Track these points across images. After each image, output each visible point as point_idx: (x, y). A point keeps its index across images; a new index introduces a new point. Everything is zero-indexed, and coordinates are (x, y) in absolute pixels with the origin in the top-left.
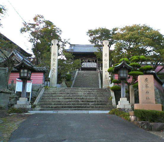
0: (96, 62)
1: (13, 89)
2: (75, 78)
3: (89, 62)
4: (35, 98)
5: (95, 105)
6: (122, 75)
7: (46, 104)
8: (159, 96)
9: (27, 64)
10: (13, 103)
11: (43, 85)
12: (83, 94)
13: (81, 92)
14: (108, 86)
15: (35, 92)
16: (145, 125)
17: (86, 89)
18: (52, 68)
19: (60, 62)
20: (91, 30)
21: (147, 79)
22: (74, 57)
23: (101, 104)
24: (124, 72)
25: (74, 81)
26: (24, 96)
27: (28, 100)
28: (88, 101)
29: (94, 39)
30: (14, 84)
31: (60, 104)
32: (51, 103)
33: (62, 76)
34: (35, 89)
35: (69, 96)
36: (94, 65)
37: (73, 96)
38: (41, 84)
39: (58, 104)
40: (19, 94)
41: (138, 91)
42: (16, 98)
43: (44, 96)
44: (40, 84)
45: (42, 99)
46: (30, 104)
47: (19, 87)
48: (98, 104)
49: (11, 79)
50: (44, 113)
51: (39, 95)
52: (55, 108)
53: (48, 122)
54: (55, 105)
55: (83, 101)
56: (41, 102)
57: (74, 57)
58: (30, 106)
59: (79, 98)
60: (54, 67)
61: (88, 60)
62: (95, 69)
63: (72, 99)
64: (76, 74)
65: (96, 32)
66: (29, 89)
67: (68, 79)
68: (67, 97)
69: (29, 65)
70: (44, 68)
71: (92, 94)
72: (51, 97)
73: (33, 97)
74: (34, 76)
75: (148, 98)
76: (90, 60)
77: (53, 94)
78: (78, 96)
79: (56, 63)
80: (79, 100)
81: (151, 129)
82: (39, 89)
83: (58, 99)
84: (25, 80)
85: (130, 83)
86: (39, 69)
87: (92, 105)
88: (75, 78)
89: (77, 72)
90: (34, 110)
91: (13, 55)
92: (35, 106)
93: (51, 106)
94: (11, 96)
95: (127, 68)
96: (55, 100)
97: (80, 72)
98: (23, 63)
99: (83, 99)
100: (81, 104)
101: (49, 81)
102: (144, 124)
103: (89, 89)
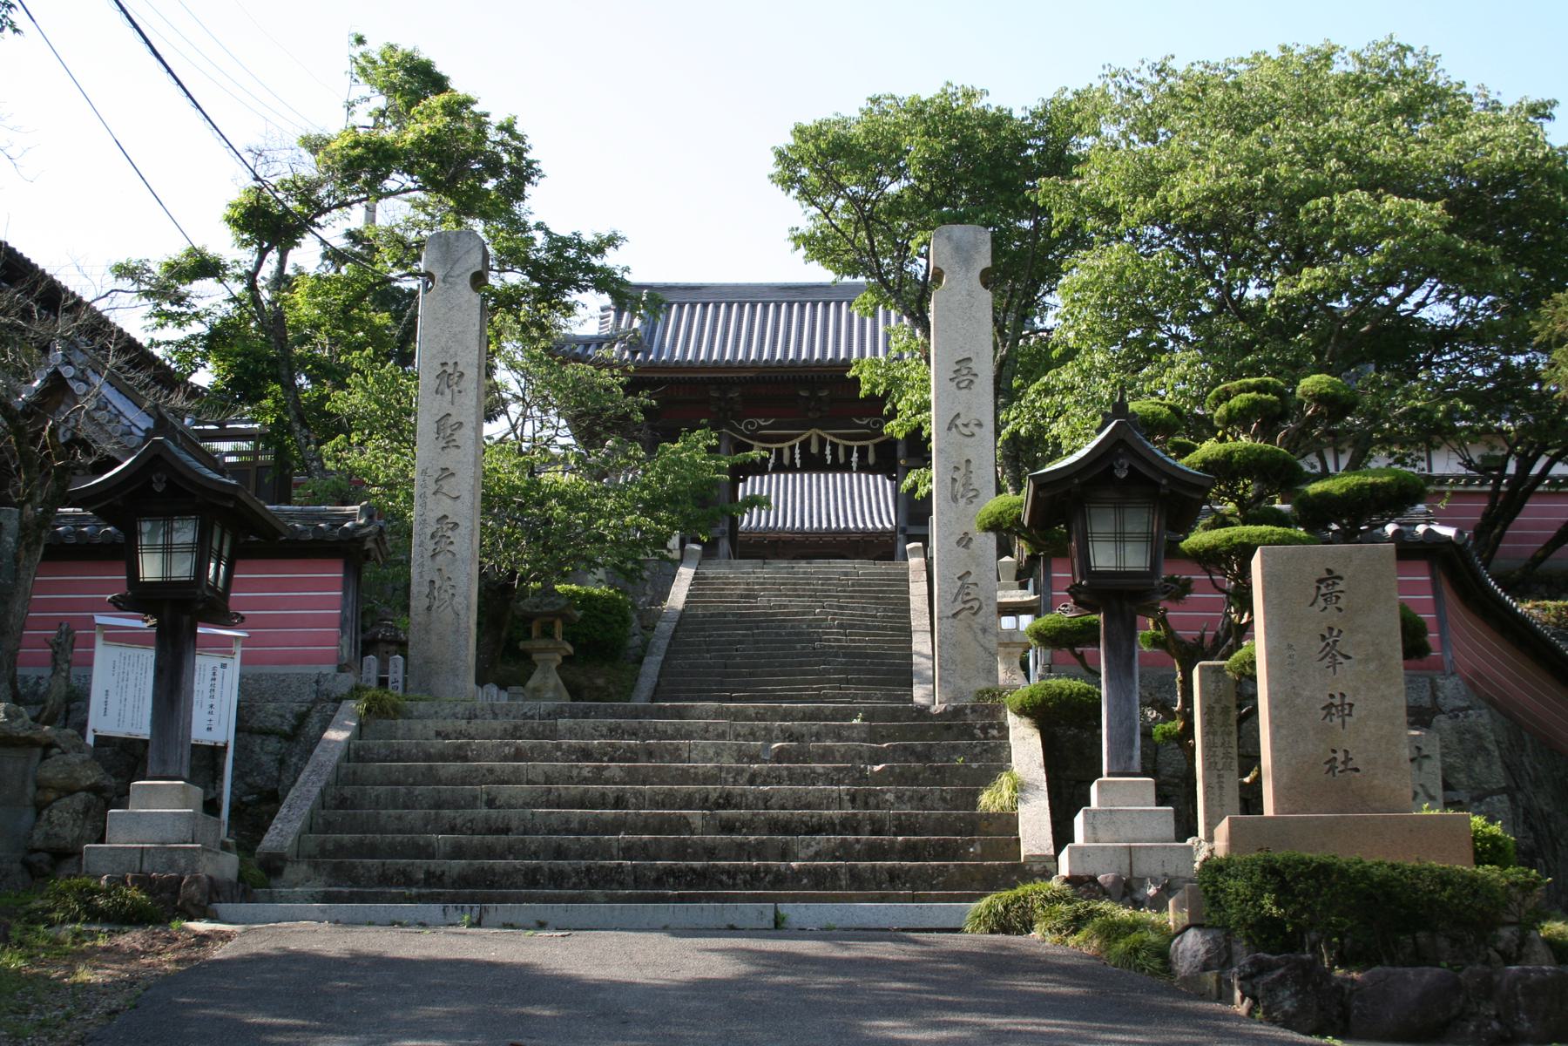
1: (75, 703)
3: (814, 464)
4: (272, 798)
5: (846, 852)
6: (1103, 558)
7: (373, 851)
8: (1498, 768)
9: (195, 464)
10: (69, 833)
11: (347, 680)
12: (728, 762)
13: (713, 743)
15: (273, 744)
16: (1281, 981)
17: (760, 717)
21: (1331, 577)
22: (646, 410)
23: (911, 851)
24: (1128, 528)
25: (651, 667)
26: (171, 772)
27: (211, 807)
28: (775, 826)
30: (74, 670)
31: (509, 851)
32: (421, 839)
34: (273, 713)
35: (598, 777)
36: (862, 501)
37: (632, 777)
38: (329, 669)
39: (490, 853)
40: (126, 760)
41: (1250, 690)
42: (95, 789)
43: (354, 779)
44: (313, 670)
45: (341, 798)
46: (225, 847)
47: (120, 692)
48: (875, 852)
49: (45, 623)
51: (308, 769)
52: (464, 880)
53: (526, 306)
54: (457, 852)
55: (728, 827)
56: (329, 827)
57: (646, 410)
58: (227, 865)
59: (690, 796)
60: (446, 506)
61: (805, 446)
62: (879, 546)
63: (619, 802)
66: (213, 713)
68: (576, 789)
69: (216, 476)
71: (825, 756)
72: (419, 789)
73: (252, 788)
74: (260, 588)
75: (1340, 756)
77: (443, 757)
78: (685, 777)
80: (695, 815)
81: (1347, 1020)
82: (302, 718)
83: (491, 803)
84: (178, 618)
85: (1208, 642)
86: (303, 516)
87: (817, 856)
90: (272, 901)
91: (57, 387)
92: (273, 867)
93: (419, 866)
94: (52, 771)
95: (1158, 485)
96: (460, 816)
98: (158, 457)
99: (727, 801)
100: (711, 852)
101: (402, 647)
102: (1281, 971)
103: (786, 716)
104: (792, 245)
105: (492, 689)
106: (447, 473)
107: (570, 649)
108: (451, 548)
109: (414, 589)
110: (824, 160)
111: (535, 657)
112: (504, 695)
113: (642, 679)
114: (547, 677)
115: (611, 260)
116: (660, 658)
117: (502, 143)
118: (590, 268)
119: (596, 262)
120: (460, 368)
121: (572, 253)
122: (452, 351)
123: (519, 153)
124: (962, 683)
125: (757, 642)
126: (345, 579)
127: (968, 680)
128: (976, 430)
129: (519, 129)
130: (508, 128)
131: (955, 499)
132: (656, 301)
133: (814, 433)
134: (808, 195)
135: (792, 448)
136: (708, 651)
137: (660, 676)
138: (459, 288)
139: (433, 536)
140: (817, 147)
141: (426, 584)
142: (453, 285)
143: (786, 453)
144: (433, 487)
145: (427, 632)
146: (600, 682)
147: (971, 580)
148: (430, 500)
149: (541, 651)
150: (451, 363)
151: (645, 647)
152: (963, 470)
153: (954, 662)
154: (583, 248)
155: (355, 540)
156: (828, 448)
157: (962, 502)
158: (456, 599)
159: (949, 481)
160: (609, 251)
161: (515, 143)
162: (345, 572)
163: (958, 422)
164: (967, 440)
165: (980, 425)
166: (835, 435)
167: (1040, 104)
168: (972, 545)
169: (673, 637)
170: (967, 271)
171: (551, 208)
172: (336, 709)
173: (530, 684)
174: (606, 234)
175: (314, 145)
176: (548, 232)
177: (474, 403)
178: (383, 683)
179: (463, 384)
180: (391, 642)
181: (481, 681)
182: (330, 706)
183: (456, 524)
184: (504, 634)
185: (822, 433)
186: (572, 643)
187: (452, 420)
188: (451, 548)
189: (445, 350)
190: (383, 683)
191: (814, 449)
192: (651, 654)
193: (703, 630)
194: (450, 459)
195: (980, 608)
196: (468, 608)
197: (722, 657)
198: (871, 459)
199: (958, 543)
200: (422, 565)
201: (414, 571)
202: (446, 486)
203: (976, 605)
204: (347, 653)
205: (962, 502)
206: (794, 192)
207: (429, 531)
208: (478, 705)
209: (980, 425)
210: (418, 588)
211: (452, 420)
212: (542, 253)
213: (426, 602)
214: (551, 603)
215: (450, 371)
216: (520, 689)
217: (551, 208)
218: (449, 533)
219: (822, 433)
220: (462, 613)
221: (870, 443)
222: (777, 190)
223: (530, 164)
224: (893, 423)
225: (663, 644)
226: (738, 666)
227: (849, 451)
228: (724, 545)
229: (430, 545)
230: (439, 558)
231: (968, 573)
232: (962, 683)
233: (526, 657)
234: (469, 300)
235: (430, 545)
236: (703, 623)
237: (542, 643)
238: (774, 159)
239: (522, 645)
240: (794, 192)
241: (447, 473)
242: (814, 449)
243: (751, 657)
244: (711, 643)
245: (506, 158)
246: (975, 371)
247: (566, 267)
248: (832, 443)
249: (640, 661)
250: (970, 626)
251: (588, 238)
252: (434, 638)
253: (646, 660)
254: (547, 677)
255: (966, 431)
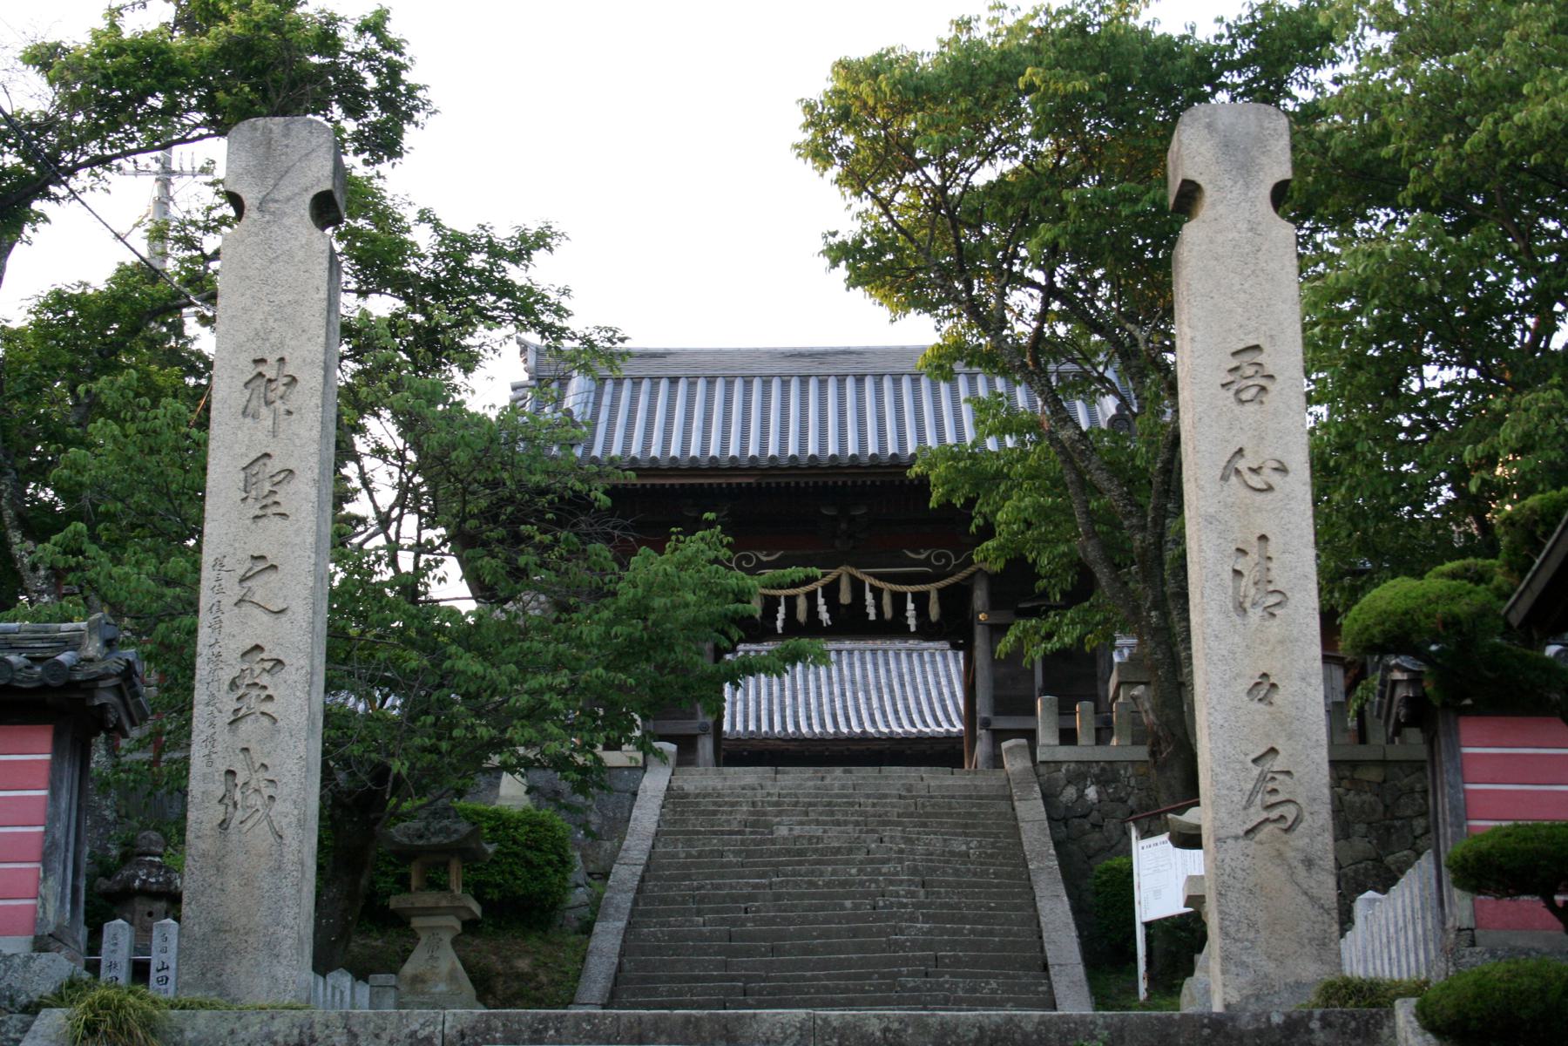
0: (952, 627)
2: (626, 874)
14: (1311, 971)
18: (222, 635)
19: (368, 631)
20: (875, 68)
25: (608, 938)
29: (949, 212)
33: (399, 832)
50: (1293, 420)
60: (258, 628)
64: (646, 815)
65: (971, 87)
67: (521, 905)
70: (83, 640)
76: (857, 587)
79: (299, 639)
88: (626, 874)
89: (655, 782)
97: (704, 778)
101: (172, 900)
104: (827, 262)
105: (342, 980)
106: (262, 565)
107: (476, 908)
108: (268, 707)
109: (195, 786)
110: (881, 118)
111: (416, 922)
112: (364, 991)
113: (593, 961)
114: (437, 958)
115: (539, 273)
116: (622, 924)
117: (368, 56)
118: (505, 289)
119: (515, 274)
120: (290, 369)
121: (477, 260)
122: (274, 338)
123: (395, 70)
124: (1270, 967)
125: (778, 897)
126: (55, 765)
127: (1280, 962)
128: (1275, 479)
129: (393, 30)
130: (374, 26)
131: (1241, 609)
132: (605, 362)
133: (844, 572)
134: (856, 180)
135: (811, 597)
136: (699, 913)
137: (622, 955)
138: (287, 221)
139: (233, 685)
140: (876, 91)
141: (220, 777)
142: (277, 216)
143: (802, 605)
144: (236, 592)
145: (219, 870)
146: (523, 964)
147: (1278, 764)
148: (230, 616)
149: (428, 912)
150: (272, 359)
151: (596, 907)
152: (1254, 555)
153: (1252, 925)
154: (495, 251)
155: (73, 686)
156: (869, 597)
157: (1255, 615)
158: (278, 806)
159: (1228, 576)
160: (539, 255)
161: (385, 55)
162: (57, 750)
163: (1242, 465)
164: (1259, 497)
165: (1282, 469)
166: (876, 576)
167: (1246, 12)
168: (1277, 698)
169: (639, 890)
170: (1247, 186)
171: (435, 184)
172: (25, 1029)
173: (408, 969)
174: (533, 228)
175: (43, 58)
176: (437, 226)
177: (316, 433)
178: (140, 971)
179: (297, 398)
180: (156, 896)
181: (322, 965)
182: (16, 1020)
183: (279, 662)
184: (364, 882)
185: (858, 574)
186: (478, 898)
187: (274, 466)
188: (268, 707)
189: (262, 335)
190: (140, 971)
191: (845, 597)
192: (606, 917)
193: (688, 877)
194: (267, 538)
195: (1298, 820)
196: (301, 824)
197: (723, 922)
198: (934, 612)
199: (1250, 692)
200: (211, 740)
201: (197, 753)
202: (261, 588)
203: (1290, 812)
204: (55, 913)
205: (1255, 615)
206: (835, 171)
207: (227, 675)
208: (318, 1016)
209: (1282, 469)
210: (203, 783)
211: (274, 466)
212: (428, 263)
213: (219, 813)
214: (445, 831)
215: (270, 373)
216: (391, 979)
217: (435, 184)
218: (264, 679)
219: (858, 574)
220: (289, 834)
221: (932, 588)
222: (807, 167)
223: (411, 90)
224: (990, 544)
225: (624, 900)
226: (751, 937)
227: (898, 600)
228: (706, 747)
229: (229, 703)
230: (245, 727)
231: (1273, 751)
232: (1270, 967)
233: (399, 922)
234: (309, 244)
235: (229, 703)
236: (685, 866)
237: (429, 899)
238: (802, 118)
239: (394, 902)
240: (835, 171)
241: (262, 565)
242: (845, 597)
243: (772, 921)
244: (702, 900)
245: (371, 82)
246: (1269, 370)
247: (465, 287)
248: (873, 589)
249: (587, 929)
250: (1280, 854)
251: (503, 233)
252: (233, 883)
253: (598, 927)
254: (437, 958)
255: (1255, 481)
